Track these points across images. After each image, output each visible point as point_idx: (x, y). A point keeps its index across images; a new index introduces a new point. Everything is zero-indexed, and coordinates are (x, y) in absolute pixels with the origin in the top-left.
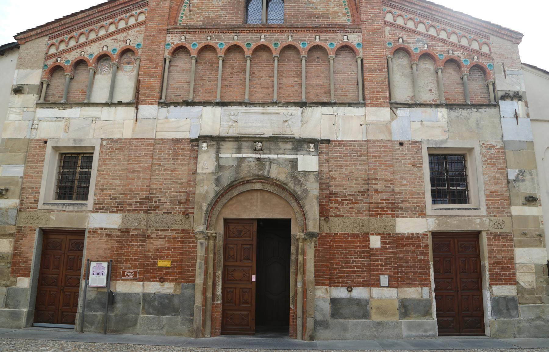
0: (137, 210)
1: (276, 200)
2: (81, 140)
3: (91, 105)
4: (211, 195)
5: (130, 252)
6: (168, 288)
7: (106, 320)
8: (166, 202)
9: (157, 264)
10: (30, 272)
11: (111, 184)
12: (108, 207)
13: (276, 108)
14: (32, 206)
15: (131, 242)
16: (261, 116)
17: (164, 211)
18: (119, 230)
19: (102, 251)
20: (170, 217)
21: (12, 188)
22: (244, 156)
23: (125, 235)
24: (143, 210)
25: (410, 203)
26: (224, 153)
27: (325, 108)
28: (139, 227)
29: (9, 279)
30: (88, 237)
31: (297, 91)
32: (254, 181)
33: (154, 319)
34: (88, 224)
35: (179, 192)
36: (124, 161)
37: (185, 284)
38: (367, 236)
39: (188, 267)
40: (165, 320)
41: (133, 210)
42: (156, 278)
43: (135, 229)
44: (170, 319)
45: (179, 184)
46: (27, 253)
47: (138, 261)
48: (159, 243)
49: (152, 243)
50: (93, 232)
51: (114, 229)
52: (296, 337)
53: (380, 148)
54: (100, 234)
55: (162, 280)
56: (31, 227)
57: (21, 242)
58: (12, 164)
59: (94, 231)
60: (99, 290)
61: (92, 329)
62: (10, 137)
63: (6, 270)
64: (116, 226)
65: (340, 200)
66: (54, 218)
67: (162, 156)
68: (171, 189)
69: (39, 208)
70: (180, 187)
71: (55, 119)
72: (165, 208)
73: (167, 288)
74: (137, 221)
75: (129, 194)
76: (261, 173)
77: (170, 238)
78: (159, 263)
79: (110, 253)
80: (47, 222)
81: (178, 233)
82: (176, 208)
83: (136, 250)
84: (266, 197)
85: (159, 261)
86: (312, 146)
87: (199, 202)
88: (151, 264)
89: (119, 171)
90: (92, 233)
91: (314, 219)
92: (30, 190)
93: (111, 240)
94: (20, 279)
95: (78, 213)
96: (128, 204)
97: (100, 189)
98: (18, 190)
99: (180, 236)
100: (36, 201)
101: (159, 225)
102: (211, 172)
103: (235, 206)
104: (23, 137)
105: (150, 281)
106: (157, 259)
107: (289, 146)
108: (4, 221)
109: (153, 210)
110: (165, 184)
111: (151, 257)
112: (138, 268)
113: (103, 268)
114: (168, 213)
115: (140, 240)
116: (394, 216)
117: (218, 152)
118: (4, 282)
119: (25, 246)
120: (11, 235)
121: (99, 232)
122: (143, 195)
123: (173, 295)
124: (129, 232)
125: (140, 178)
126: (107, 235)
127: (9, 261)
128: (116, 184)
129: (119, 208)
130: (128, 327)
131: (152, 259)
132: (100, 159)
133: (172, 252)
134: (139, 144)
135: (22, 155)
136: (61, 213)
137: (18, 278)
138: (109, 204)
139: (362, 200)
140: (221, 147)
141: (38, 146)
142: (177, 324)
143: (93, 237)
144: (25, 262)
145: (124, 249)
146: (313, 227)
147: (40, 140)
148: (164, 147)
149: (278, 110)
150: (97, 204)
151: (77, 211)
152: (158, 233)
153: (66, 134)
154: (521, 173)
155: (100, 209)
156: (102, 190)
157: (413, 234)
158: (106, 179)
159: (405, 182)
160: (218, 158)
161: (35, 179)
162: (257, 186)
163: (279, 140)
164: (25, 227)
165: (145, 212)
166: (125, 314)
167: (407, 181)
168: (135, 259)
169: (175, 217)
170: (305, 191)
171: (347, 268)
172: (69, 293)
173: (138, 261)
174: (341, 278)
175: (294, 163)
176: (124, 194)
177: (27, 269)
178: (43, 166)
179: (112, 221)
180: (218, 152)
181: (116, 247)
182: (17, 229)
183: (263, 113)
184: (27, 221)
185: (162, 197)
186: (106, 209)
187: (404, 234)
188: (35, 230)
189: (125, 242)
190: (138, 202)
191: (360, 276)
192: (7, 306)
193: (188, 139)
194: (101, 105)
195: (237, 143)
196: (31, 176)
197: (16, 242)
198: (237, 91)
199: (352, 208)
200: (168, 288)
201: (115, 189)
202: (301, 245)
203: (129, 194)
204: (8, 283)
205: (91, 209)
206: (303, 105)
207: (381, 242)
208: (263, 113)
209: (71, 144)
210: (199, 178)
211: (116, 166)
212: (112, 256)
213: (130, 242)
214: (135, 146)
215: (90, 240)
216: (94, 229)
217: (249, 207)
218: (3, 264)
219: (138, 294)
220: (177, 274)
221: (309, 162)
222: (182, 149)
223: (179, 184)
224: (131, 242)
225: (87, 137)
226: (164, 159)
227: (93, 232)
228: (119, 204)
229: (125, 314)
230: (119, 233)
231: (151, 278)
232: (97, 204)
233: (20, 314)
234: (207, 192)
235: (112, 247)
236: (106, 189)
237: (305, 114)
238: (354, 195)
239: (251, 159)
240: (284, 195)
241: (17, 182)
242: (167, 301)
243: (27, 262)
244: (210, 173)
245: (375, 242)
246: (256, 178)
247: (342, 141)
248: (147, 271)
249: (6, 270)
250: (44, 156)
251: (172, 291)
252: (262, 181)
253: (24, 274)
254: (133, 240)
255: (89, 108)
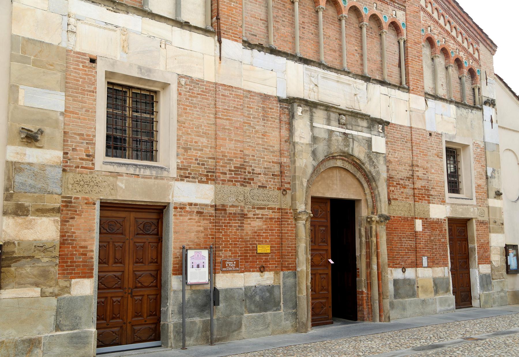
0: (232, 181)
1: (350, 179)
2: (149, 71)
3: (157, 18)
4: (310, 170)
5: (229, 235)
6: (267, 278)
7: (208, 327)
8: (260, 174)
9: (257, 250)
10: (93, 269)
11: (196, 142)
12: (196, 174)
13: (347, 78)
14: (84, 164)
15: (229, 223)
16: (335, 84)
17: (259, 185)
18: (212, 206)
19: (193, 234)
20: (266, 192)
21: (47, 130)
22: (333, 128)
23: (221, 213)
24: (239, 181)
25: (436, 191)
26: (316, 122)
27: (382, 87)
28: (236, 204)
29: (57, 284)
30: (175, 215)
31: (357, 61)
32: (338, 157)
33: (259, 317)
34: (173, 197)
35: (273, 162)
36: (209, 113)
37: (286, 272)
38: (414, 218)
39: (288, 253)
40: (269, 317)
41: (229, 181)
42: (256, 268)
43: (233, 206)
44: (275, 315)
45: (272, 152)
46: (85, 240)
47: (238, 247)
48: (257, 224)
49: (250, 224)
50: (181, 208)
51: (206, 205)
52: (374, 320)
53: (420, 137)
54: (190, 212)
55: (262, 269)
56: (87, 199)
57: (71, 222)
58: (43, 87)
59: (181, 207)
60: (194, 288)
61: (191, 342)
62: (30, 37)
63: (52, 269)
64: (208, 202)
65: (395, 183)
66: (123, 186)
67: (252, 114)
68: (264, 158)
69: (97, 168)
70: (273, 156)
71: (103, 25)
72: (260, 181)
73: (267, 279)
74: (233, 196)
75: (221, 159)
76: (346, 149)
77: (267, 218)
78: (258, 248)
79: (204, 238)
80: (112, 191)
81: (275, 212)
82: (270, 181)
83: (235, 232)
84: (343, 176)
85: (258, 246)
86: (381, 126)
87: (299, 177)
88: (250, 250)
89: (205, 126)
90: (179, 210)
91: (385, 202)
92: (78, 137)
93: (204, 219)
94: (76, 283)
95: (157, 181)
96: (222, 173)
97: (183, 148)
98: (59, 136)
99: (277, 215)
100: (90, 157)
101: (256, 202)
102: (308, 143)
103: (320, 183)
104: (55, 43)
105: (250, 271)
106: (256, 244)
107: (365, 124)
108: (39, 186)
109: (248, 182)
110: (257, 150)
111: (249, 241)
112: (239, 256)
113: (204, 257)
114: (263, 187)
115: (239, 220)
116: (429, 203)
117: (311, 121)
118: (51, 290)
119: (80, 229)
120: (58, 210)
121: (188, 208)
122: (237, 162)
123: (273, 287)
124: (225, 210)
125: (232, 140)
126: (198, 212)
127: (57, 253)
128: (202, 143)
129: (210, 177)
130: (233, 332)
131: (251, 244)
132: (178, 104)
133: (270, 236)
134: (227, 93)
135: (59, 76)
136: (133, 179)
137: (73, 281)
138: (196, 170)
139: (408, 185)
140: (314, 114)
141: (81, 65)
142: (281, 320)
143: (180, 215)
144: (83, 254)
145: (221, 232)
146: (384, 209)
147: (84, 54)
148: (252, 102)
149: (349, 80)
150: (181, 169)
151: (156, 178)
152: (255, 211)
153: (125, 55)
154: (494, 170)
155: (186, 177)
156: (186, 149)
157: (438, 219)
158: (190, 134)
159: (433, 171)
160: (312, 127)
161: (85, 119)
162: (339, 163)
163: (359, 116)
164: (78, 198)
165: (242, 185)
166: (228, 316)
167: (435, 171)
168: (235, 244)
169: (271, 193)
170: (378, 173)
171: (402, 250)
172: (140, 298)
173: (238, 247)
174: (398, 260)
175: (369, 142)
176: (214, 158)
177: (87, 266)
178: (95, 100)
179: (202, 194)
180: (311, 121)
181: (210, 229)
182: (63, 201)
183: (338, 81)
184: (78, 189)
185: (255, 167)
186: (193, 178)
187: (434, 219)
188: (94, 204)
189: (223, 223)
190: (232, 171)
191: (409, 257)
192: (58, 328)
193: (275, 97)
194: (170, 22)
195: (326, 112)
196: (76, 114)
197: (64, 222)
198: (310, 47)
199: (402, 192)
200: (267, 278)
201: (202, 150)
202: (374, 227)
203: (221, 159)
204: (56, 290)
205: (175, 176)
206: (367, 79)
207: (423, 225)
208: (338, 81)
209: (135, 74)
210: (298, 148)
211: (200, 119)
212: (206, 241)
213: (228, 223)
214: (223, 95)
215: (177, 219)
216: (180, 204)
217: (331, 185)
218: (47, 259)
219: (241, 289)
220: (276, 261)
221: (379, 144)
222: (270, 108)
223: (272, 152)
224: (229, 223)
225: (158, 68)
226: (254, 118)
227: (181, 208)
228: (209, 172)
229: (228, 316)
230: (212, 211)
231: (251, 267)
232: (181, 169)
233: (87, 337)
234: (306, 166)
235: (206, 229)
236: (190, 149)
237: (369, 91)
238: (404, 180)
239: (338, 133)
240: (358, 175)
241: (57, 121)
242: (268, 294)
243: (86, 255)
244: (307, 144)
245: (419, 226)
246: (342, 154)
247: (395, 124)
248: (250, 261)
249: (52, 269)
250: (94, 84)
251: (272, 282)
252: (344, 158)
253: (83, 273)
254: (231, 220)
255: (153, 22)
